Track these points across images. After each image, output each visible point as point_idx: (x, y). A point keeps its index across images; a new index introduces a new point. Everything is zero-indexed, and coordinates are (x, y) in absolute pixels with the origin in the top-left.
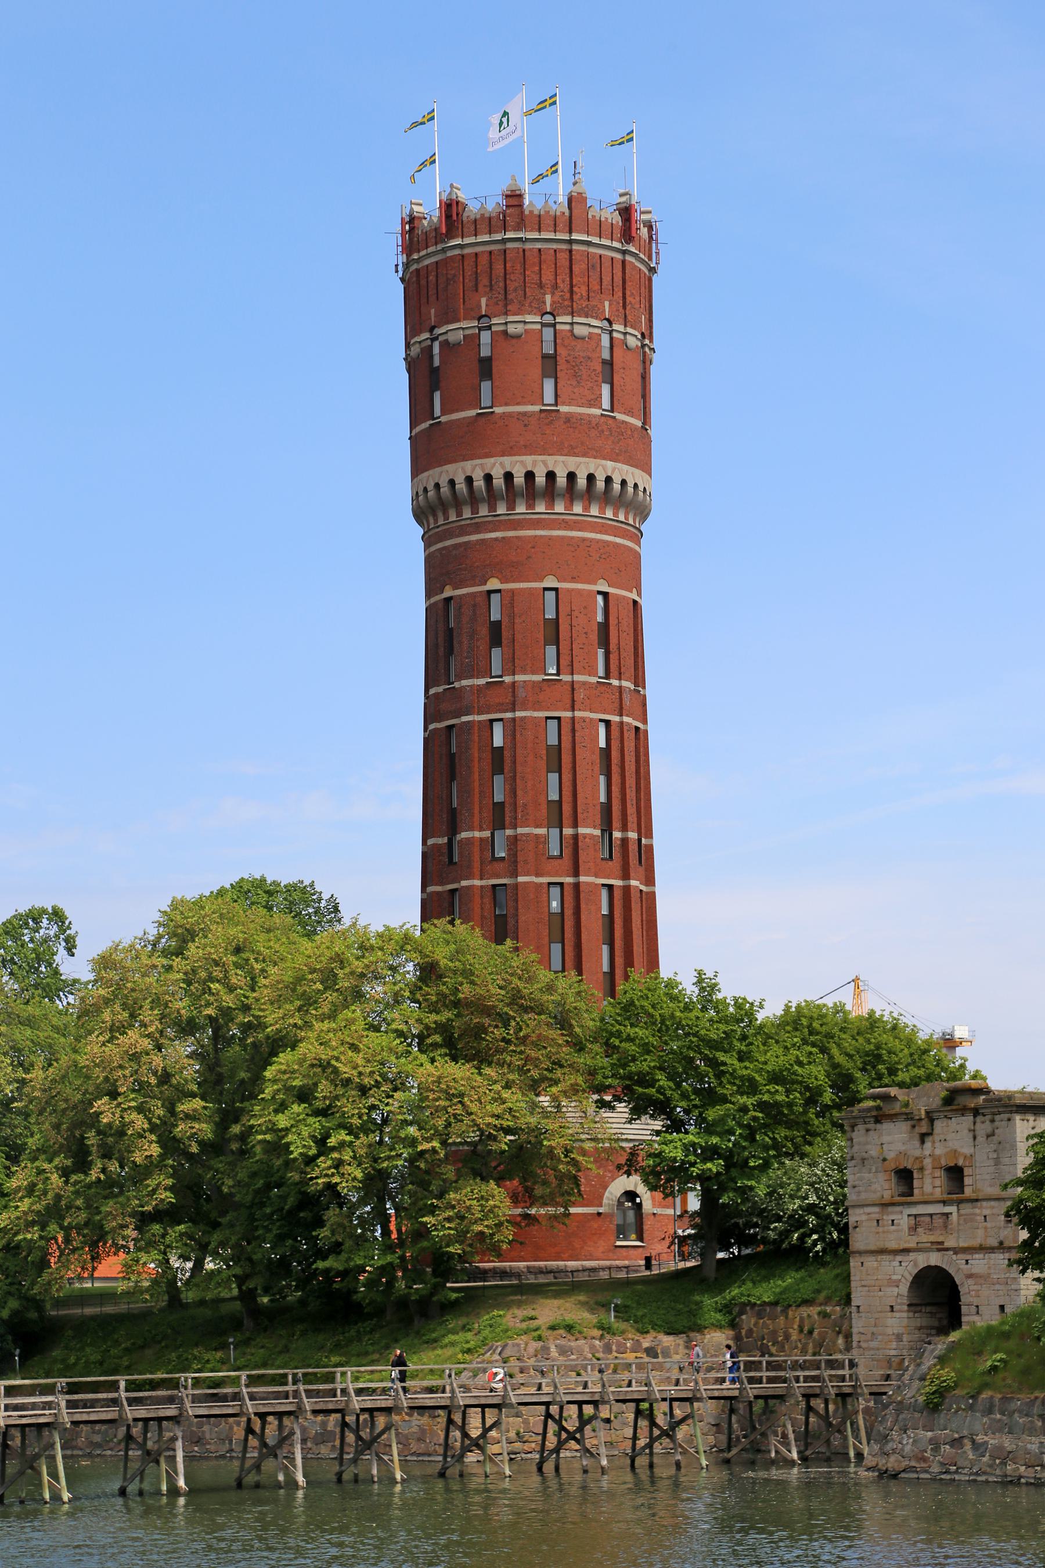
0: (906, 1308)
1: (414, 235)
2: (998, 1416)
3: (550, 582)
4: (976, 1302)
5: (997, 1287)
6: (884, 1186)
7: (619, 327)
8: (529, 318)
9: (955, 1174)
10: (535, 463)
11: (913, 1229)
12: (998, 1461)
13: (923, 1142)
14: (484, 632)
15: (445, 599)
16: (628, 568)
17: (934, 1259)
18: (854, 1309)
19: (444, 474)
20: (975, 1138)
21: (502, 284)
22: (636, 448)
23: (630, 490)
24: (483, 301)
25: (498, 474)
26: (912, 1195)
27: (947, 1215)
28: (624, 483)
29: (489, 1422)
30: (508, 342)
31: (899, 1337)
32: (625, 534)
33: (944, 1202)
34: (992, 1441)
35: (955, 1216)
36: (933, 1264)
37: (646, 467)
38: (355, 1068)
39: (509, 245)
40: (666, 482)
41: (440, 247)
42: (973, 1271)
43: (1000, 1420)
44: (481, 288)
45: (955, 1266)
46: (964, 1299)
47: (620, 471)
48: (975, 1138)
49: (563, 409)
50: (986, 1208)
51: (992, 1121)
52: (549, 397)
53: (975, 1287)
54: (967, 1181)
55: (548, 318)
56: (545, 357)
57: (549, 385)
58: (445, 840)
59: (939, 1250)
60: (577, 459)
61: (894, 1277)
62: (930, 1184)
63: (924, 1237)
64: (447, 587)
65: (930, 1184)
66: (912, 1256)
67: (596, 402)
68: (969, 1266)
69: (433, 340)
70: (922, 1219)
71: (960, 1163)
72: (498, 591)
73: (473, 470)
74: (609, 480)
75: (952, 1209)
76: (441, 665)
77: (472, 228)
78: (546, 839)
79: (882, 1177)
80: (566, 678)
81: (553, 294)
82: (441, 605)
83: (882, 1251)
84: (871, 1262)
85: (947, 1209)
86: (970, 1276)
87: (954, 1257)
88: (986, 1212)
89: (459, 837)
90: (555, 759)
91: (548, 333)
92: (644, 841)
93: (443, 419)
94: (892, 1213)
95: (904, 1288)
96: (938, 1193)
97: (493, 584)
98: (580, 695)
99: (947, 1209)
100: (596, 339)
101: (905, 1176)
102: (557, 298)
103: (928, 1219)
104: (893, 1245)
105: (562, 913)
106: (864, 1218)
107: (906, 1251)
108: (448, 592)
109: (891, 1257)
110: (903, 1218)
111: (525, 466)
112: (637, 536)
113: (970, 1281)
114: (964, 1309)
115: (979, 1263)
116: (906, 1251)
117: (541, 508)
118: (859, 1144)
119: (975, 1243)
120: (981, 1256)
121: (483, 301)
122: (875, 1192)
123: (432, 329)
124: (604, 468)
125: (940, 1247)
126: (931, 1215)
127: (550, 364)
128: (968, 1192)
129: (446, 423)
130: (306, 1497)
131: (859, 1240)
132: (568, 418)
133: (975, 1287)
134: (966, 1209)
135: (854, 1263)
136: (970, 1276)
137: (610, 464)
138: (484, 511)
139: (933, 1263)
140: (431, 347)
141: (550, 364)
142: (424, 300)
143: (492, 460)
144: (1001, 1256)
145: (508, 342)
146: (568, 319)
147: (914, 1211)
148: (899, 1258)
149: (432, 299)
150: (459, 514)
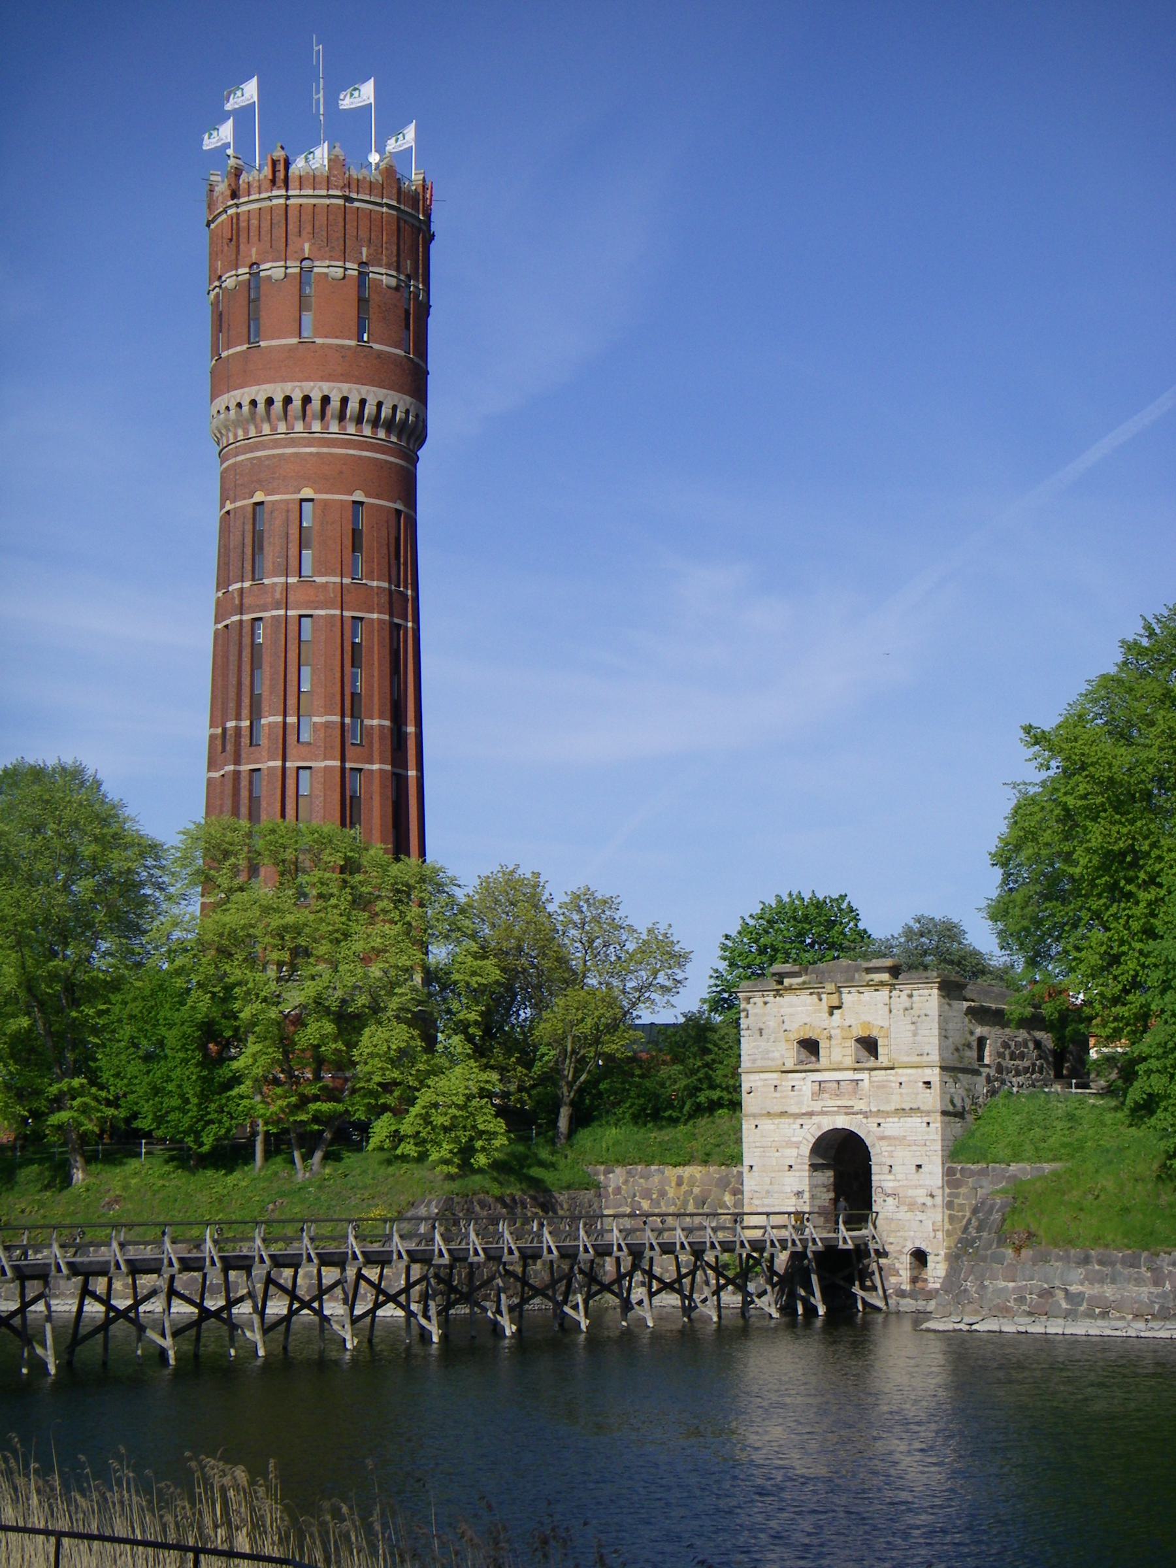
0: (807, 1167)
2: (1097, 1267)
5: (914, 1148)
6: (789, 1055)
9: (869, 1045)
10: (350, 390)
12: (1097, 1310)
13: (831, 1014)
15: (354, 502)
17: (842, 1122)
19: (261, 393)
20: (891, 1011)
21: (324, 233)
24: (307, 246)
29: (30, 1295)
31: (799, 1194)
34: (1089, 1290)
35: (866, 1082)
36: (840, 1127)
38: (1075, 926)
42: (887, 1134)
43: (1098, 1271)
44: (304, 233)
45: (864, 1128)
46: (874, 1159)
48: (891, 1011)
50: (903, 1074)
51: (911, 996)
53: (889, 1148)
59: (847, 1114)
60: (332, 384)
61: (794, 1139)
62: (839, 1052)
63: (829, 1102)
64: (258, 493)
65: (839, 1052)
66: (815, 1119)
68: (881, 1129)
70: (827, 1085)
71: (874, 1034)
72: (311, 500)
73: (293, 390)
75: (864, 1076)
77: (297, 183)
79: (783, 1046)
81: (369, 247)
82: (250, 509)
83: (783, 1114)
84: (767, 1125)
85: (858, 1076)
86: (882, 1138)
87: (864, 1120)
89: (263, 721)
94: (792, 1079)
96: (849, 1061)
97: (307, 493)
99: (858, 1076)
101: (810, 1046)
102: (371, 251)
103: (835, 1085)
106: (759, 1084)
107: (811, 1114)
108: (259, 497)
109: (791, 1120)
110: (805, 1083)
111: (359, 393)
113: (883, 1143)
114: (874, 1169)
115: (892, 1126)
116: (811, 1114)
118: (756, 1015)
120: (896, 1119)
121: (307, 246)
122: (773, 1060)
124: (321, 389)
125: (849, 1111)
126: (838, 1082)
129: (266, 347)
133: (889, 1148)
136: (882, 1138)
142: (243, 239)
143: (312, 384)
144: (919, 1120)
147: (818, 1076)
148: (800, 1121)
149: (254, 238)
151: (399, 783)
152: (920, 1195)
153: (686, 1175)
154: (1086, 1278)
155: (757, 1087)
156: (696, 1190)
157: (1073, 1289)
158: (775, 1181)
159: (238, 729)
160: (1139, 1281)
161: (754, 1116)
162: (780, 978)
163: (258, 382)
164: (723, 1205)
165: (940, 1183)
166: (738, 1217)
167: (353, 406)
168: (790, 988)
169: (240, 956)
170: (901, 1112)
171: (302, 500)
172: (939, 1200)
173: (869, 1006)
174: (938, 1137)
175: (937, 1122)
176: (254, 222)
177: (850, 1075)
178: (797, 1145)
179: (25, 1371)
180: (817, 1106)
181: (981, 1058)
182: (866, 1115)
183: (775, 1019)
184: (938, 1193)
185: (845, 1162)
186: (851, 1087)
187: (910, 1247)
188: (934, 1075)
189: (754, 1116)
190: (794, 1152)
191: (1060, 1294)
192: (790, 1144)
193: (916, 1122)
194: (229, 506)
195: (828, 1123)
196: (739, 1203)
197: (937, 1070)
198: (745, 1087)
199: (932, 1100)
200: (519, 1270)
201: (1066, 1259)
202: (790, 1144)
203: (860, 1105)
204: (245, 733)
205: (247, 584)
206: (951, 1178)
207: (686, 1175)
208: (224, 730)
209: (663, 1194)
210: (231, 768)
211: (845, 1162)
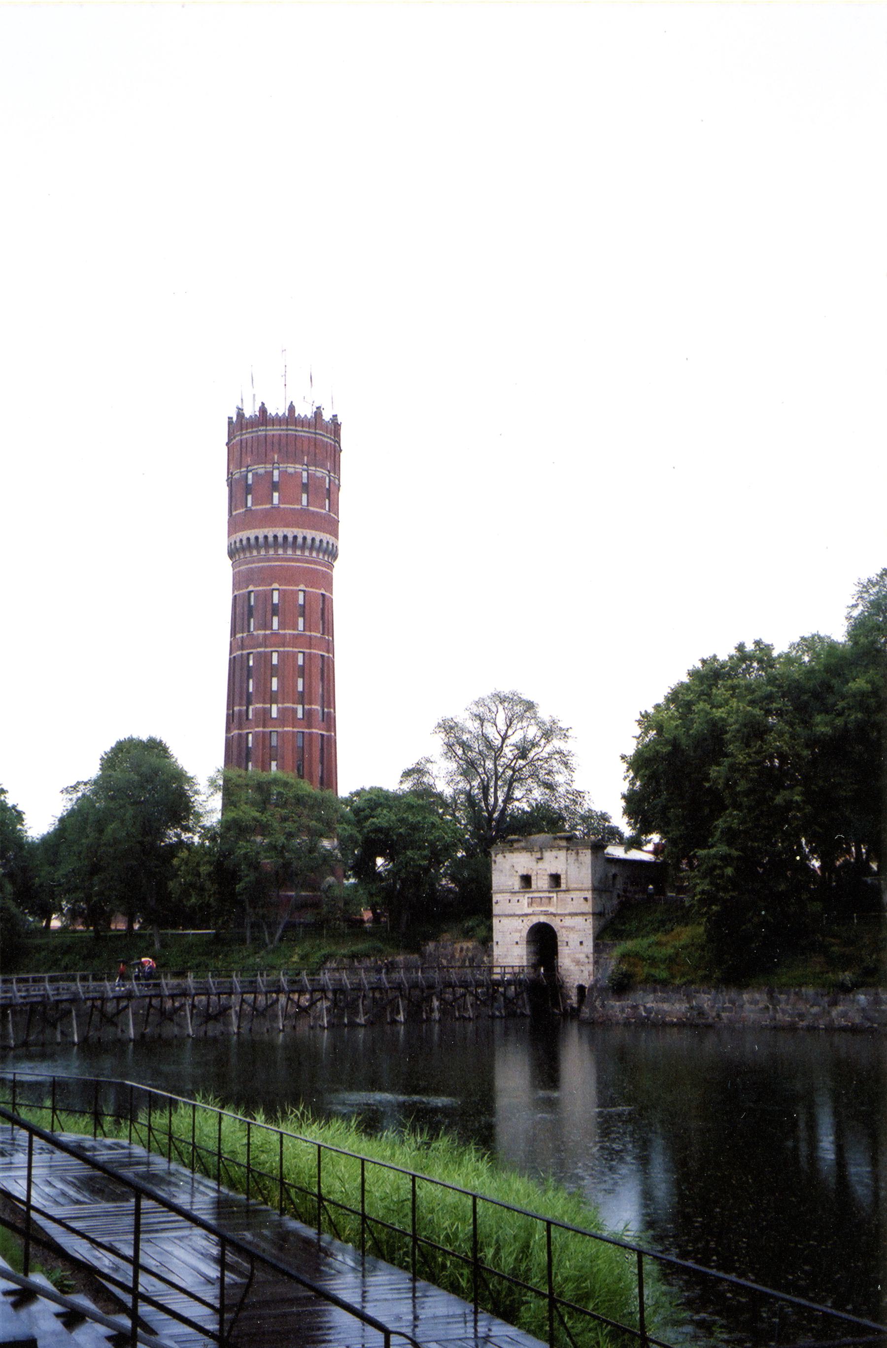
1: (238, 425)
3: (302, 587)
4: (566, 940)
6: (517, 884)
7: (332, 474)
8: (297, 466)
11: (530, 904)
14: (269, 608)
16: (327, 581)
17: (543, 919)
18: (495, 943)
22: (331, 525)
23: (331, 546)
24: (276, 457)
25: (280, 535)
26: (531, 887)
27: (550, 898)
28: (328, 543)
30: (283, 468)
32: (324, 565)
33: (549, 892)
37: (336, 536)
39: (290, 432)
40: (346, 542)
41: (254, 429)
45: (555, 923)
46: (559, 938)
47: (319, 536)
49: (311, 508)
50: (574, 894)
52: (305, 502)
54: (533, 882)
55: (305, 467)
56: (303, 484)
57: (304, 496)
58: (245, 708)
62: (541, 882)
65: (541, 882)
66: (529, 917)
67: (323, 507)
69: (248, 471)
72: (278, 589)
74: (321, 541)
75: (554, 895)
76: (246, 622)
78: (295, 711)
80: (308, 633)
84: (505, 921)
85: (551, 895)
88: (574, 896)
90: (302, 671)
91: (305, 474)
92: (326, 710)
93: (253, 508)
95: (525, 933)
97: (275, 586)
98: (313, 642)
100: (323, 478)
101: (526, 880)
104: (519, 912)
105: (303, 747)
110: (525, 900)
112: (331, 566)
113: (563, 930)
114: (559, 943)
115: (568, 921)
116: (526, 915)
117: (299, 553)
119: (567, 912)
121: (276, 457)
123: (247, 467)
126: (541, 898)
127: (305, 488)
128: (534, 886)
130: (407, 1032)
131: (496, 909)
132: (313, 513)
134: (561, 895)
135: (495, 921)
137: (322, 534)
138: (272, 552)
139: (542, 921)
140: (247, 475)
141: (305, 488)
145: (283, 468)
146: (314, 468)
147: (531, 895)
150: (259, 552)
151: (323, 610)
152: (582, 957)
153: (465, 947)
154: (654, 1000)
155: (501, 903)
156: (470, 954)
157: (648, 1005)
158: (510, 950)
159: (240, 711)
160: (681, 1000)
161: (499, 916)
162: (512, 842)
163: (309, 527)
164: (483, 962)
165: (592, 951)
166: (491, 968)
167: (300, 540)
168: (517, 849)
169: (430, 1216)
170: (573, 915)
171: (274, 589)
172: (591, 960)
173: (556, 861)
174: (591, 926)
175: (590, 920)
176: (249, 444)
177: (547, 894)
178: (520, 931)
179: (798, 858)
180: (530, 911)
181: (614, 884)
182: (555, 915)
183: (507, 867)
184: (591, 956)
185: (543, 939)
186: (547, 901)
187: (576, 984)
188: (589, 895)
189: (499, 916)
190: (518, 934)
191: (642, 1008)
192: (516, 931)
193: (579, 920)
194: (236, 593)
195: (535, 920)
196: (491, 962)
197: (590, 892)
198: (494, 900)
199: (588, 908)
200: (458, 995)
201: (645, 991)
202: (516, 931)
203: (552, 910)
204: (244, 713)
205: (245, 635)
206: (598, 948)
207: (465, 947)
208: (233, 711)
209: (453, 956)
210: (236, 732)
211: (543, 939)
